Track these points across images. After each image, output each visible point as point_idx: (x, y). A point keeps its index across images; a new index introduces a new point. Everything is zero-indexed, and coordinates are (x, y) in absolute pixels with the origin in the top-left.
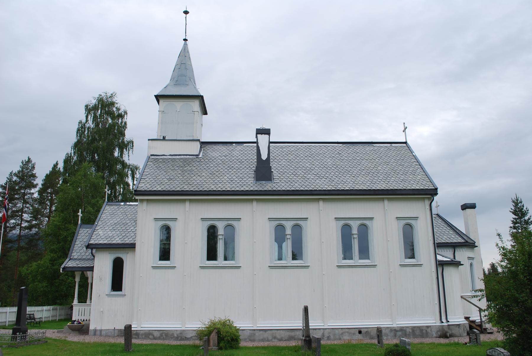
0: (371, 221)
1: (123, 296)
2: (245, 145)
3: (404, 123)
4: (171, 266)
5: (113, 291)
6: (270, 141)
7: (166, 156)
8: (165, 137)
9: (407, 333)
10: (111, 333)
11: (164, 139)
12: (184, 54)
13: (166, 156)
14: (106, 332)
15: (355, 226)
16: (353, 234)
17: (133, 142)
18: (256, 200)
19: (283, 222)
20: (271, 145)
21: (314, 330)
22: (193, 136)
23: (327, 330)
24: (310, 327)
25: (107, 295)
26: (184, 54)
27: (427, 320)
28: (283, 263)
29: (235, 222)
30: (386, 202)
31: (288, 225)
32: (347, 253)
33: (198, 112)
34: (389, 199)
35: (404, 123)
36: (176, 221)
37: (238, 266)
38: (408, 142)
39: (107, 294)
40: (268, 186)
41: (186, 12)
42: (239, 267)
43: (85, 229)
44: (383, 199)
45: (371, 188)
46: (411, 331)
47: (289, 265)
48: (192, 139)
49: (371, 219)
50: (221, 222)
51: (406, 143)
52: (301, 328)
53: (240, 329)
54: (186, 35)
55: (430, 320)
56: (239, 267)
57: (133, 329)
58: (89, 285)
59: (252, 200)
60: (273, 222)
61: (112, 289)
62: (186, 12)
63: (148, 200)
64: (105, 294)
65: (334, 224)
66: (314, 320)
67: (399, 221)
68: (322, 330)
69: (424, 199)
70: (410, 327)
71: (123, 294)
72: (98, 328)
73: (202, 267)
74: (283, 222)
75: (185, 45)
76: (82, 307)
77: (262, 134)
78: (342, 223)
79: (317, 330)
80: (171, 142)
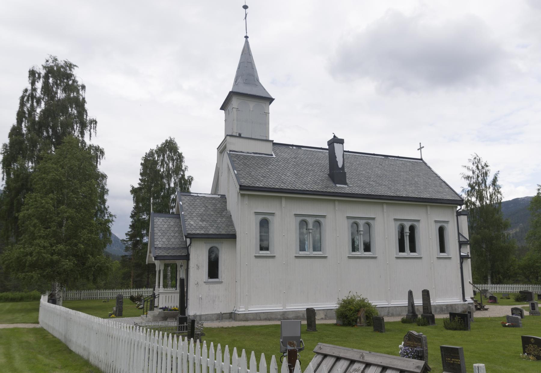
0: (418, 223)
1: (221, 283)
2: (303, 148)
3: (420, 143)
4: (323, 255)
5: (210, 278)
6: (344, 150)
7: (244, 153)
8: (241, 134)
9: (443, 309)
10: (210, 318)
11: (240, 136)
12: (246, 52)
13: (244, 153)
14: (205, 317)
15: (407, 225)
16: (360, 231)
17: (96, 122)
18: (338, 200)
19: (358, 221)
20: (345, 153)
21: (382, 308)
22: (266, 136)
23: (391, 307)
24: (415, 305)
25: (205, 282)
26: (246, 52)
27: (455, 300)
28: (357, 254)
29: (321, 218)
30: (429, 208)
31: (361, 223)
32: (402, 249)
33: (233, 109)
34: (431, 206)
35: (420, 143)
36: (273, 215)
37: (273, 255)
38: (423, 159)
39: (205, 281)
40: (341, 188)
41: (245, 7)
42: (325, 257)
43: (160, 218)
44: (426, 205)
45: (270, 186)
46: (445, 308)
47: (312, 255)
48: (265, 139)
49: (324, 216)
50: (311, 218)
51: (421, 159)
52: (407, 305)
53: (377, 306)
54: (247, 33)
55: (456, 300)
56: (325, 257)
57: (431, 304)
58: (157, 273)
59: (334, 200)
60: (350, 220)
61: (208, 277)
62: (245, 7)
63: (249, 195)
64: (203, 282)
65: (433, 224)
66: (381, 300)
67: (436, 223)
68: (387, 308)
69: (453, 208)
70: (445, 305)
71: (221, 281)
72: (198, 314)
73: (297, 257)
74: (358, 221)
75: (247, 43)
76: (169, 295)
77: (337, 143)
78: (261, 217)
79: (384, 308)
80: (248, 140)
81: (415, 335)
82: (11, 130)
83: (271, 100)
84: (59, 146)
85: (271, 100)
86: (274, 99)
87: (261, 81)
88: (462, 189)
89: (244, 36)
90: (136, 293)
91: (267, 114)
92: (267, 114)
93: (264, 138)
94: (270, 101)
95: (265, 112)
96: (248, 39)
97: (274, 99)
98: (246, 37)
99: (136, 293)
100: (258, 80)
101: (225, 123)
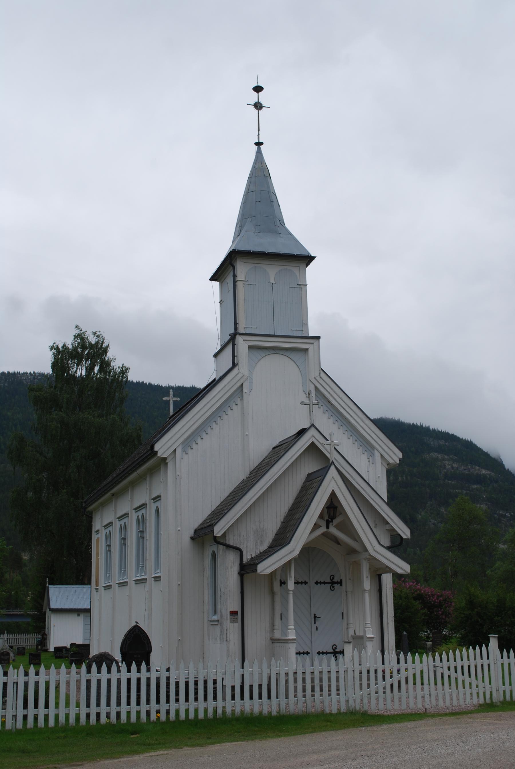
62: (258, 89)
81: (209, 591)
82: (489, 454)
83: (309, 259)
84: (490, 474)
85: (309, 259)
86: (314, 258)
87: (287, 225)
88: (77, 332)
89: (264, 144)
90: (10, 641)
91: (302, 286)
92: (302, 286)
93: (300, 334)
94: (307, 262)
95: (299, 284)
96: (261, 146)
97: (314, 258)
98: (259, 144)
99: (10, 641)
100: (282, 223)
101: (221, 306)
